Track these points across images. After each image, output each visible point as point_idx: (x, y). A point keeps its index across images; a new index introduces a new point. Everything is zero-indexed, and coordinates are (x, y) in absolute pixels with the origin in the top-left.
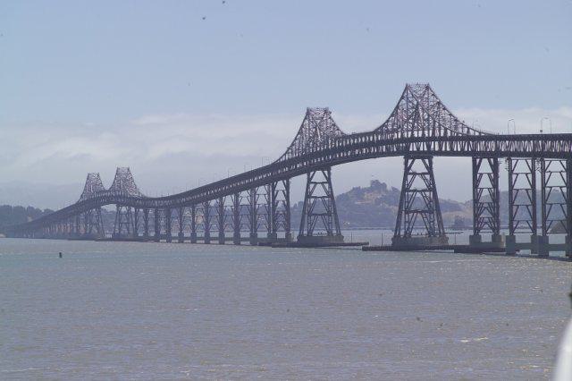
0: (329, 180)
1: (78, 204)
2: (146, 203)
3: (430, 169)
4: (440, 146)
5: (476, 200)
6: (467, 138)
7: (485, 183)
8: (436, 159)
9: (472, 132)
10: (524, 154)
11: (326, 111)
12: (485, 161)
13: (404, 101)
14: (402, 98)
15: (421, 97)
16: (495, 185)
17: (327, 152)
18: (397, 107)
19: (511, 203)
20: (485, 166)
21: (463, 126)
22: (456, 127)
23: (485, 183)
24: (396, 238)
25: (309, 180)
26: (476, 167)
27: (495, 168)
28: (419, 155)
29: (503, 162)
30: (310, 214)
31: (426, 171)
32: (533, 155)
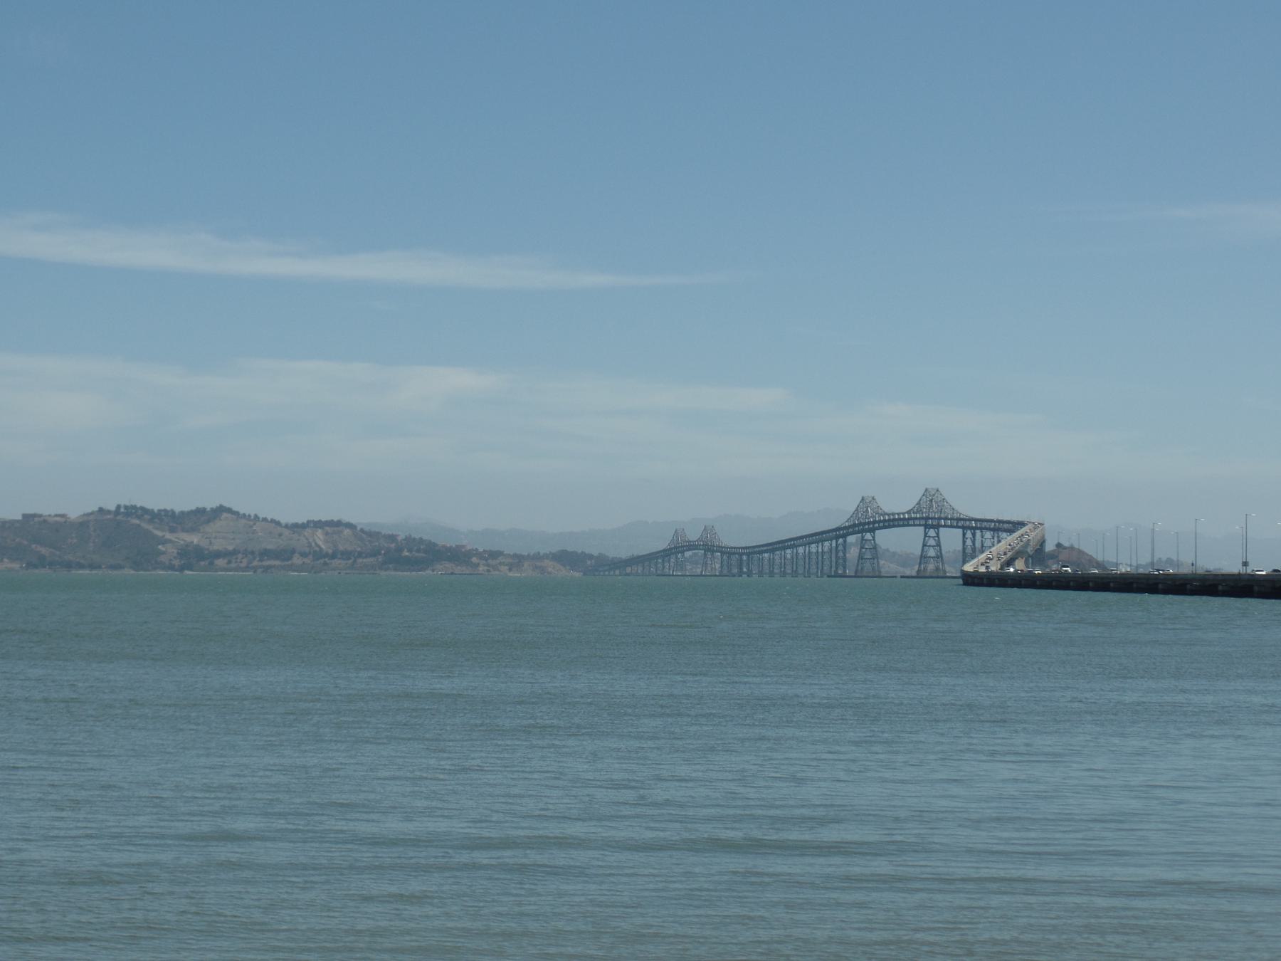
0: (938, 536)
1: (664, 551)
2: (728, 552)
3: (938, 534)
4: (957, 524)
5: (964, 549)
6: (959, 519)
7: (969, 543)
8: (941, 529)
9: (962, 516)
10: (989, 529)
11: (873, 498)
12: (868, 534)
13: (924, 497)
14: (924, 495)
15: (934, 495)
16: (974, 544)
17: (875, 522)
18: (920, 500)
19: (797, 558)
20: (969, 534)
21: (958, 512)
22: (953, 513)
23: (969, 543)
24: (919, 571)
25: (863, 537)
26: (964, 535)
27: (974, 535)
28: (933, 527)
29: (978, 533)
30: (862, 559)
31: (871, 538)
32: (994, 530)
